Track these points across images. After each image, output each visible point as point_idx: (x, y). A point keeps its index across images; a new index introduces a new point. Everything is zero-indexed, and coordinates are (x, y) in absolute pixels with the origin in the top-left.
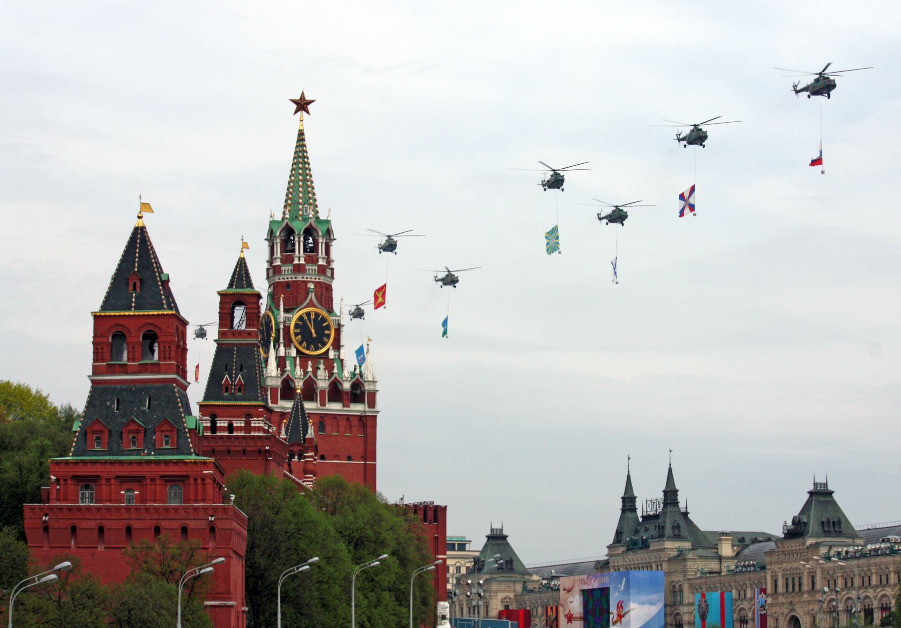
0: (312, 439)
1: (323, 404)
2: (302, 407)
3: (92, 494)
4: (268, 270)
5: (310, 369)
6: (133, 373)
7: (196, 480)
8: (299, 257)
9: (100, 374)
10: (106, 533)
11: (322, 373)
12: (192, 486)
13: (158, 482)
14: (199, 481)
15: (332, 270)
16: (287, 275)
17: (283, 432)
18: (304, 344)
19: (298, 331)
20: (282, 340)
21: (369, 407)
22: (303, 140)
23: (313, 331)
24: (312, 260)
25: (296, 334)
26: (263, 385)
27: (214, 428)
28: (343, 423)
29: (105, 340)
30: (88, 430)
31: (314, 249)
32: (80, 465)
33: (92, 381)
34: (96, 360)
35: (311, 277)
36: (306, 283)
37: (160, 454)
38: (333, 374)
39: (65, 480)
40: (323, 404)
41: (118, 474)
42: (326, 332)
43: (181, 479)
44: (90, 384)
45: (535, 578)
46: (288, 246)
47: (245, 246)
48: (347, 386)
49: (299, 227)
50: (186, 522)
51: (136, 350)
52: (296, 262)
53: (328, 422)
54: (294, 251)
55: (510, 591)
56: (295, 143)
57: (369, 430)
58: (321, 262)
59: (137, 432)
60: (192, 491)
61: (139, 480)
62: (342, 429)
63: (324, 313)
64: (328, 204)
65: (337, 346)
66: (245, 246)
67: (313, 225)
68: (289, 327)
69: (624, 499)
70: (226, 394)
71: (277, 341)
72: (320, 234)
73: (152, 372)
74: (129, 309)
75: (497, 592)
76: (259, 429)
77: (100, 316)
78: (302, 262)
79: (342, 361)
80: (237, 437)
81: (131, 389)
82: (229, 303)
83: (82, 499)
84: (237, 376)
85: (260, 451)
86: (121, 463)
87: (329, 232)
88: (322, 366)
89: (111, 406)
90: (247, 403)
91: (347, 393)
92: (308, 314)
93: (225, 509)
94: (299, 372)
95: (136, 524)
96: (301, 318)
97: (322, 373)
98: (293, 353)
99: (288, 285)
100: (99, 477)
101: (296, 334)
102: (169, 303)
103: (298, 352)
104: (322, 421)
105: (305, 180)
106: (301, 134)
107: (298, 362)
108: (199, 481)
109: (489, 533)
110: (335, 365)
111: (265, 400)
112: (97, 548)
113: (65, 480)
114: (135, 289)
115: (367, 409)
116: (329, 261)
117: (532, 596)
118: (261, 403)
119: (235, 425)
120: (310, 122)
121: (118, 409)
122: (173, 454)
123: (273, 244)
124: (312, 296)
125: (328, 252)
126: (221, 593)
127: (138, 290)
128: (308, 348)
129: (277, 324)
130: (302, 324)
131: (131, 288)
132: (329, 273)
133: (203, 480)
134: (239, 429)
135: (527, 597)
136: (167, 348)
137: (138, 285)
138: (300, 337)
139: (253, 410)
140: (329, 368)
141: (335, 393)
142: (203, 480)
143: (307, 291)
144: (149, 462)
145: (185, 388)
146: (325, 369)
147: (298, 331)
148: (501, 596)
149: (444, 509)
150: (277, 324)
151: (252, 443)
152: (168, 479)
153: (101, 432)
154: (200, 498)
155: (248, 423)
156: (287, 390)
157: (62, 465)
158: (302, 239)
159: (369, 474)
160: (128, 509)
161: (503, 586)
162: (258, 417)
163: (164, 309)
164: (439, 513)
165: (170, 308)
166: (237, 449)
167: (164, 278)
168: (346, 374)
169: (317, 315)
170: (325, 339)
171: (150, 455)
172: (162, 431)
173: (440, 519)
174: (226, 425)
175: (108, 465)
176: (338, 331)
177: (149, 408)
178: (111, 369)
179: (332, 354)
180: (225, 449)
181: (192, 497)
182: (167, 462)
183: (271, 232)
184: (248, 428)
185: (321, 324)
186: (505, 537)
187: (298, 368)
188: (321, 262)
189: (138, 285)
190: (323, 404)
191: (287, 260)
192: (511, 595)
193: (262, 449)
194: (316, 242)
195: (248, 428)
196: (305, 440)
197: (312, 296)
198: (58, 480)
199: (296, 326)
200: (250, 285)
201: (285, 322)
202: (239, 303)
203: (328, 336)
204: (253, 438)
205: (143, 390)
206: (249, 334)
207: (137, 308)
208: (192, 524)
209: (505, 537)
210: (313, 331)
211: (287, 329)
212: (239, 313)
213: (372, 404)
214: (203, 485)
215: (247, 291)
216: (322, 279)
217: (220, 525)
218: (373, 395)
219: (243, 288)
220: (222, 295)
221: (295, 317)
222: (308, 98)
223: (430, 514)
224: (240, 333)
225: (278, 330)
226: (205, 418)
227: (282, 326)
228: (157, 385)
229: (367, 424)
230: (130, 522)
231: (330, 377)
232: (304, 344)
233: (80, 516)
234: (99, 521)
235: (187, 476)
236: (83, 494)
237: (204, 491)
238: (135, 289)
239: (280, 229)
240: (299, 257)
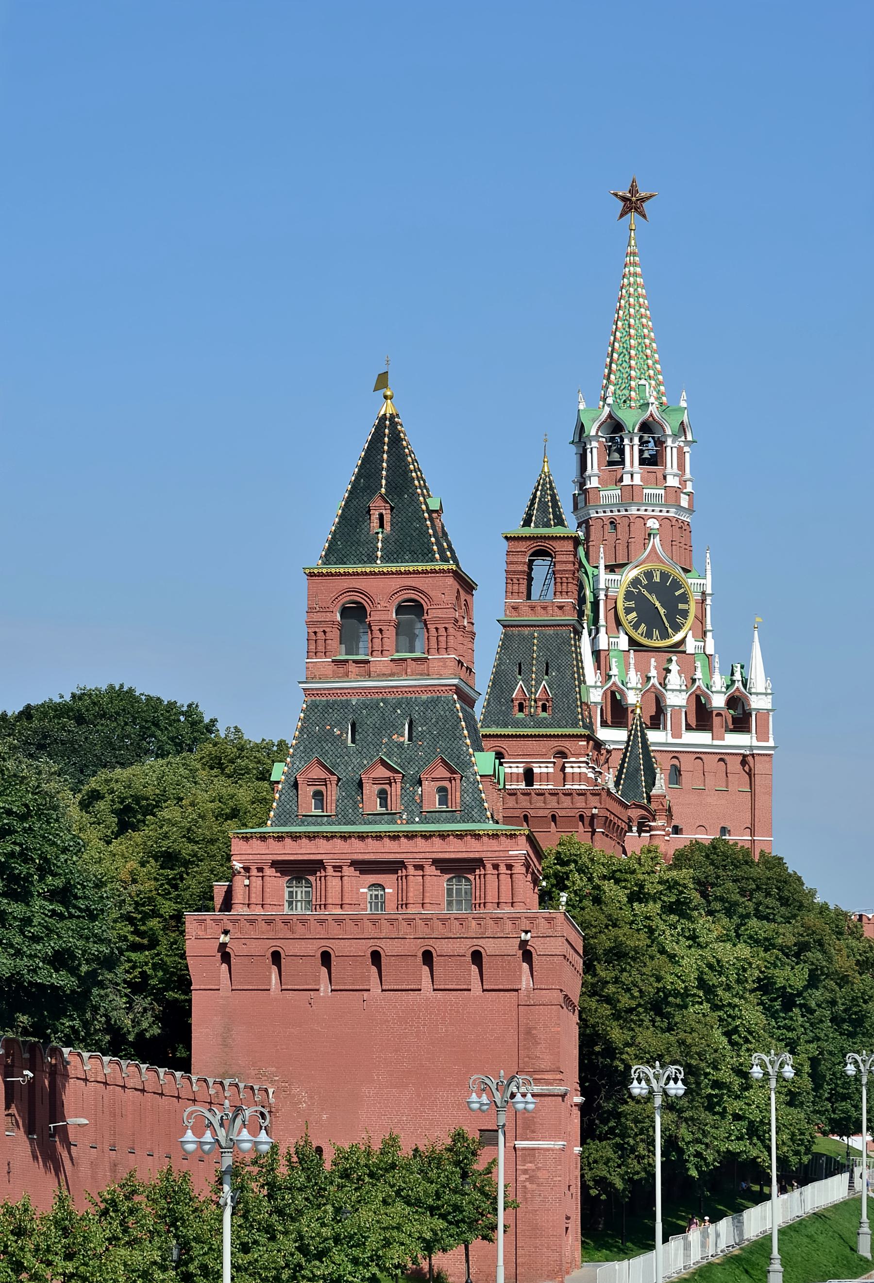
1: (677, 734)
2: (644, 736)
5: (653, 673)
7: (496, 867)
9: (321, 679)
10: (283, 961)
11: (675, 680)
14: (503, 869)
18: (643, 627)
19: (632, 604)
20: (602, 621)
21: (673, 736)
23: (658, 604)
25: (628, 611)
26: (584, 700)
28: (711, 762)
29: (328, 617)
32: (288, 841)
38: (694, 681)
39: (260, 870)
41: (356, 857)
42: (681, 606)
49: (631, 419)
50: (481, 942)
51: (386, 634)
52: (627, 480)
58: (672, 481)
63: (678, 573)
67: (657, 415)
70: (521, 715)
72: (669, 431)
74: (372, 559)
76: (581, 777)
77: (320, 575)
78: (637, 480)
80: (540, 794)
83: (290, 903)
84: (539, 683)
85: (581, 817)
89: (341, 735)
96: (635, 582)
98: (623, 642)
100: (321, 862)
101: (628, 611)
102: (442, 551)
103: (632, 642)
108: (503, 869)
110: (698, 664)
111: (590, 727)
118: (582, 731)
119: (536, 770)
121: (353, 742)
122: (454, 821)
123: (585, 450)
127: (388, 527)
128: (649, 635)
134: (547, 777)
136: (442, 632)
137: (387, 518)
138: (634, 614)
141: (702, 717)
142: (509, 867)
146: (679, 672)
147: (632, 604)
151: (566, 801)
153: (325, 782)
156: (618, 712)
158: (636, 440)
163: (433, 560)
165: (444, 559)
166: (541, 813)
174: (521, 771)
177: (410, 739)
179: (691, 646)
180: (547, 813)
187: (632, 673)
188: (672, 481)
190: (677, 734)
198: (247, 869)
199: (628, 596)
201: (607, 588)
203: (685, 614)
210: (658, 604)
219: (549, 526)
225: (595, 604)
230: (378, 942)
232: (643, 627)
236: (291, 893)
239: (596, 425)
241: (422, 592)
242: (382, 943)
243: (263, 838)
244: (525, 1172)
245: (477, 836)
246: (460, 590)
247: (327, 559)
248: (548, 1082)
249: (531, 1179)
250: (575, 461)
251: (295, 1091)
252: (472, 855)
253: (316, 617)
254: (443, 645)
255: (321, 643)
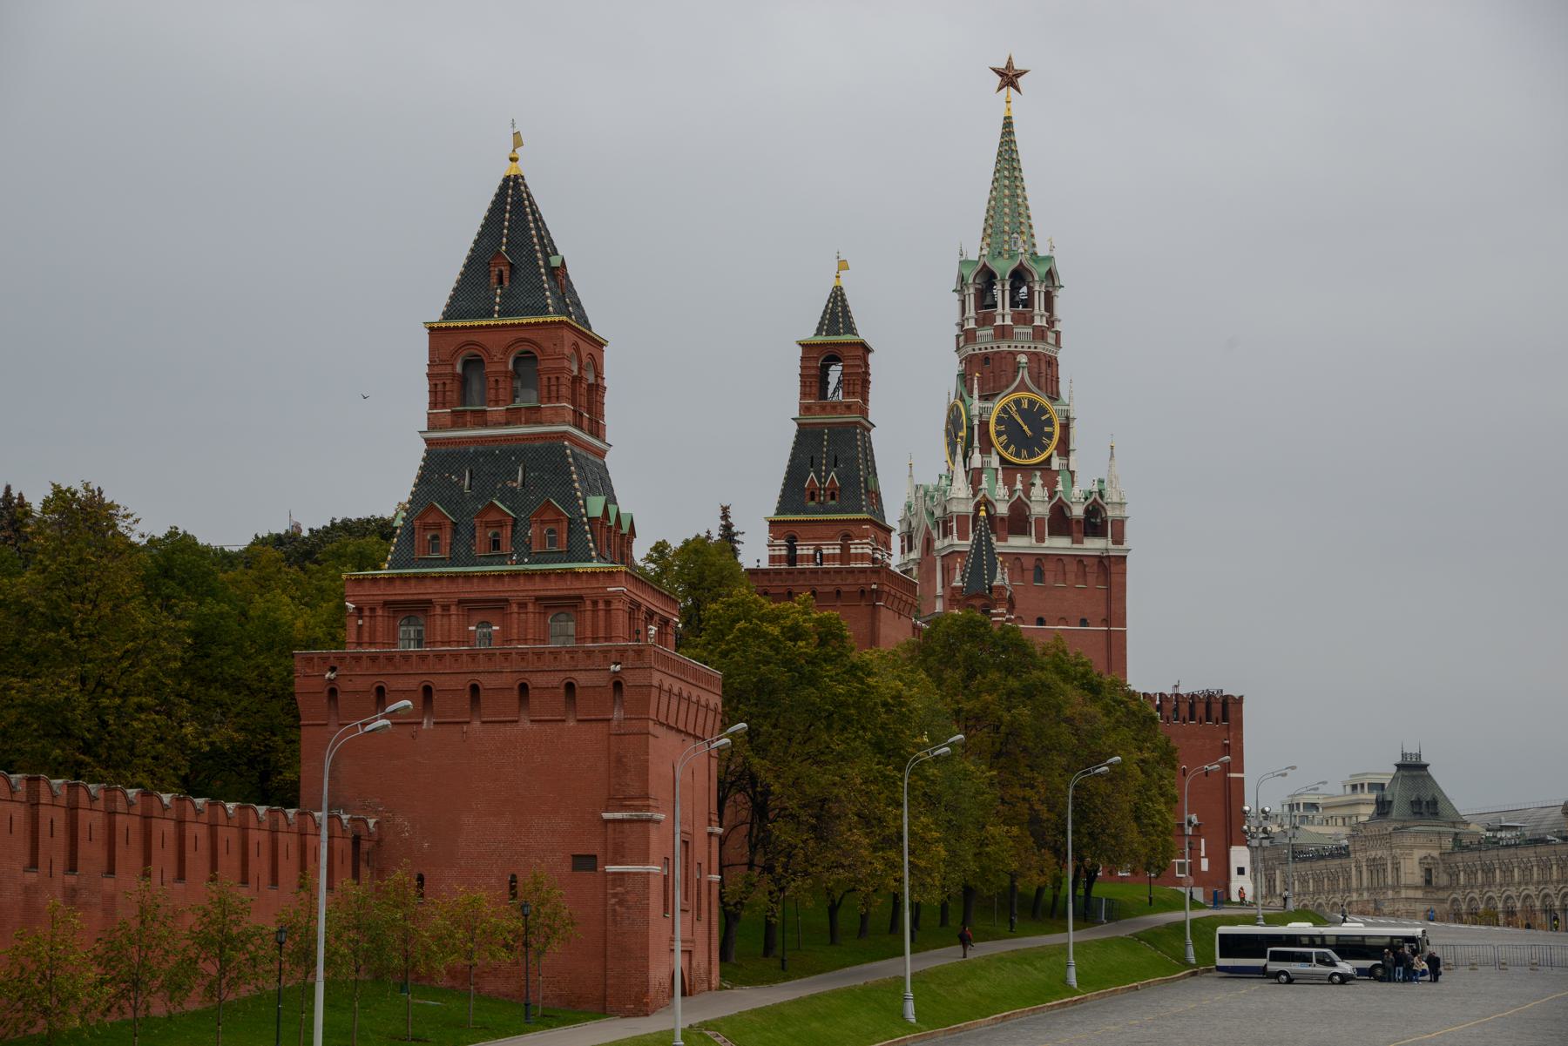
0: (1003, 587)
1: (1040, 539)
3: (419, 632)
4: (958, 337)
5: (1019, 486)
6: (497, 425)
7: (595, 603)
8: (1004, 314)
11: (1039, 492)
12: (589, 614)
13: (531, 608)
14: (601, 606)
15: (1058, 334)
16: (986, 341)
17: (958, 578)
19: (1002, 428)
22: (1011, 133)
24: (1024, 319)
27: (792, 558)
28: (1072, 567)
30: (417, 524)
31: (1028, 303)
33: (426, 440)
34: (433, 405)
35: (1021, 343)
36: (1014, 354)
37: (537, 562)
39: (372, 610)
40: (1040, 539)
41: (462, 596)
42: (1047, 429)
43: (570, 604)
44: (425, 446)
45: (1473, 827)
46: (985, 301)
47: (843, 265)
48: (1078, 511)
49: (1003, 268)
50: (573, 675)
52: (999, 322)
53: (1048, 566)
54: (995, 306)
55: (1433, 848)
56: (998, 140)
57: (1115, 579)
58: (1039, 322)
59: (500, 524)
60: (589, 623)
61: (499, 606)
62: (1071, 577)
63: (1043, 400)
64: (1053, 230)
65: (1064, 449)
66: (843, 265)
67: (1026, 264)
68: (987, 423)
69: (981, 285)
70: (812, 504)
71: (969, 444)
73: (527, 423)
74: (490, 315)
75: (1412, 847)
76: (862, 557)
77: (440, 329)
78: (1008, 322)
79: (1072, 473)
80: (802, 572)
81: (493, 453)
82: (817, 359)
84: (828, 474)
86: (468, 577)
87: (1050, 275)
88: (1038, 481)
90: (844, 517)
91: (1078, 521)
92: (1018, 402)
93: (639, 652)
94: (1001, 491)
95: (486, 681)
97: (1039, 492)
98: (995, 462)
99: (986, 359)
100: (430, 602)
101: (999, 434)
103: (1003, 460)
104: (1040, 565)
105: (1014, 196)
106: (1008, 124)
107: (1000, 476)
108: (601, 606)
109: (1399, 760)
110: (1059, 478)
112: (421, 723)
113: (372, 610)
114: (501, 281)
115: (1111, 546)
116: (1051, 322)
117: (1467, 855)
120: (1022, 105)
124: (1024, 374)
125: (1049, 306)
126: (632, 798)
127: (506, 284)
128: (1018, 455)
129: (970, 419)
130: (1005, 419)
131: (494, 280)
132: (1051, 337)
133: (608, 603)
134: (833, 557)
135: (1458, 857)
136: (553, 381)
137: (506, 274)
139: (853, 528)
140: (1050, 485)
141: (1060, 521)
143: (1017, 368)
144: (514, 575)
145: (601, 454)
147: (1002, 428)
148: (1418, 854)
149: (1239, 701)
150: (970, 419)
152: (549, 604)
154: (601, 634)
155: (845, 548)
157: (367, 584)
158: (1007, 287)
159: (1115, 647)
160: (473, 656)
161: (1421, 840)
162: (861, 538)
164: (1231, 708)
166: (827, 589)
167: (555, 261)
168: (1077, 492)
169: (1032, 403)
170: (1045, 441)
171: (522, 563)
172: (542, 522)
173: (1232, 716)
175: (445, 582)
176: (1066, 428)
178: (458, 420)
179: (1056, 463)
181: (589, 634)
182: (545, 575)
183: (962, 279)
184: (845, 556)
185: (1035, 416)
186: (1425, 767)
189: (506, 274)
191: (985, 321)
192: (1435, 853)
193: (867, 588)
194: (1031, 292)
195: (845, 556)
196: (990, 589)
197: (1024, 374)
198: (359, 610)
199: (999, 421)
200: (851, 329)
202: (834, 359)
203: (1050, 436)
204: (852, 571)
205: (514, 453)
206: (848, 407)
207: (501, 314)
208: (582, 679)
209: (1425, 767)
211: (984, 425)
212: (835, 373)
213: (1119, 539)
214: (608, 611)
215: (848, 338)
216: (1041, 347)
217: (630, 679)
218: (1120, 524)
220: (806, 347)
221: (997, 406)
222: (1017, 66)
223: (1217, 710)
224: (834, 407)
225: (970, 428)
226: (777, 542)
227: (976, 422)
228: (537, 444)
229: (1110, 570)
231: (1051, 498)
233: (392, 671)
234: (425, 678)
235: (581, 597)
237: (609, 626)
238: (501, 281)
240: (1004, 314)
241: (540, 347)
242: (481, 678)
243: (374, 580)
244: (615, 895)
245: (576, 575)
246: (581, 343)
247: (447, 315)
248: (637, 809)
249: (621, 903)
250: (958, 305)
251: (399, 820)
252: (572, 593)
253: (437, 370)
254: (554, 394)
255: (440, 395)
